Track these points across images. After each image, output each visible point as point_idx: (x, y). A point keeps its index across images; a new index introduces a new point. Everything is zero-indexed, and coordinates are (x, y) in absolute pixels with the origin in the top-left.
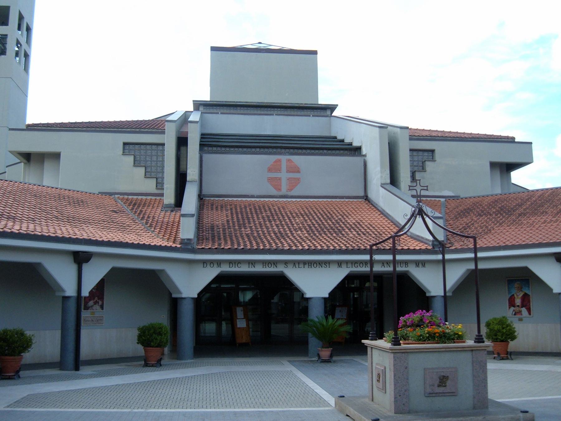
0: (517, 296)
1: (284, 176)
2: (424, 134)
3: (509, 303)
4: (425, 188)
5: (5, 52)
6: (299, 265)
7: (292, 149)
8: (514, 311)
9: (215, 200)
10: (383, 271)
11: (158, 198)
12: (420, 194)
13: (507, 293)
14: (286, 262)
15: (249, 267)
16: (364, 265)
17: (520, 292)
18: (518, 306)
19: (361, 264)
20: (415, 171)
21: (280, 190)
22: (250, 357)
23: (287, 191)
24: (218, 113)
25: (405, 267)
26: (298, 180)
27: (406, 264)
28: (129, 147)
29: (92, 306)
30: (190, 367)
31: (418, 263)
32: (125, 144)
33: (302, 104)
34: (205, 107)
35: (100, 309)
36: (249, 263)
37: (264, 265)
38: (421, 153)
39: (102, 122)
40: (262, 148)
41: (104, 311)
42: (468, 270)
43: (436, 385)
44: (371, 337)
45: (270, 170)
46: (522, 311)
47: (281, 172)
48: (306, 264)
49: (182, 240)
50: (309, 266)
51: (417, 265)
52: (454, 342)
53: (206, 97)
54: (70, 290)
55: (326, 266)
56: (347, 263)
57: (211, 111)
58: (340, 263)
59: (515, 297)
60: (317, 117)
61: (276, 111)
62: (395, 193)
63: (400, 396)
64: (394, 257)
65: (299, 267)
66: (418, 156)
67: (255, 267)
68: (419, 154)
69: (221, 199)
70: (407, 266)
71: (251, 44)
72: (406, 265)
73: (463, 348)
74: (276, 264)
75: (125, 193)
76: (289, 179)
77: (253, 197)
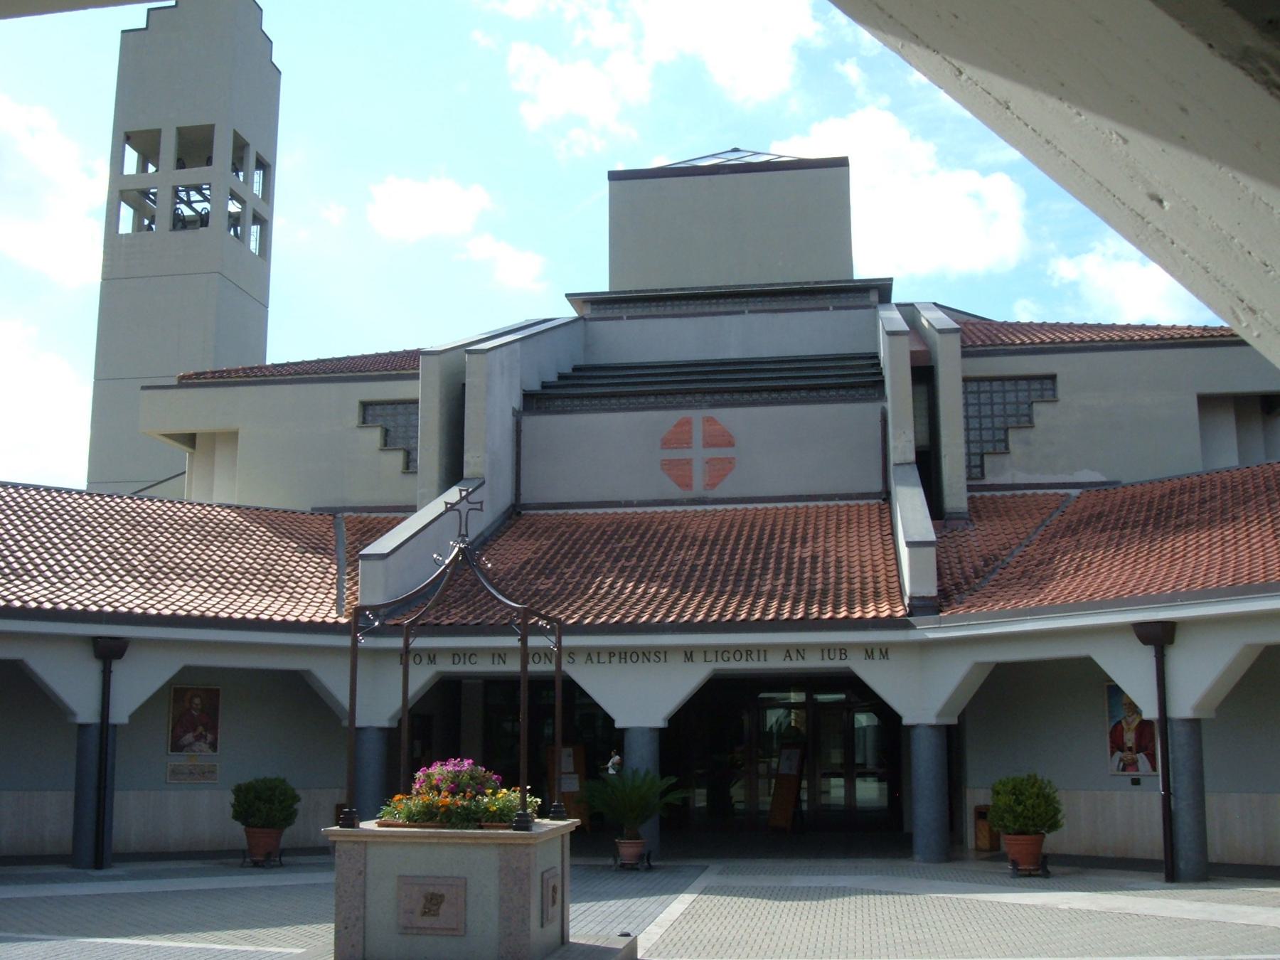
0: (1128, 724)
1: (698, 454)
2: (1115, 335)
3: (1112, 742)
5: (208, 222)
6: (705, 656)
8: (1121, 760)
13: (1107, 718)
15: (493, 663)
17: (1133, 714)
18: (1130, 749)
19: (738, 653)
21: (688, 486)
22: (845, 858)
24: (620, 318)
25: (841, 659)
27: (843, 651)
28: (991, 386)
29: (190, 744)
31: (869, 651)
32: (365, 406)
34: (595, 306)
35: (210, 750)
36: (493, 655)
40: (660, 394)
41: (218, 753)
42: (979, 665)
44: (553, 812)
45: (666, 444)
46: (1137, 761)
48: (615, 655)
50: (620, 658)
52: (481, 827)
53: (600, 283)
54: (86, 711)
55: (658, 660)
56: (705, 652)
57: (609, 313)
58: (689, 654)
59: (1123, 728)
63: (346, 928)
65: (705, 661)
67: (806, 656)
68: (1019, 388)
69: (560, 512)
70: (843, 657)
72: (841, 654)
74: (647, 655)
76: (709, 462)
77: (629, 504)
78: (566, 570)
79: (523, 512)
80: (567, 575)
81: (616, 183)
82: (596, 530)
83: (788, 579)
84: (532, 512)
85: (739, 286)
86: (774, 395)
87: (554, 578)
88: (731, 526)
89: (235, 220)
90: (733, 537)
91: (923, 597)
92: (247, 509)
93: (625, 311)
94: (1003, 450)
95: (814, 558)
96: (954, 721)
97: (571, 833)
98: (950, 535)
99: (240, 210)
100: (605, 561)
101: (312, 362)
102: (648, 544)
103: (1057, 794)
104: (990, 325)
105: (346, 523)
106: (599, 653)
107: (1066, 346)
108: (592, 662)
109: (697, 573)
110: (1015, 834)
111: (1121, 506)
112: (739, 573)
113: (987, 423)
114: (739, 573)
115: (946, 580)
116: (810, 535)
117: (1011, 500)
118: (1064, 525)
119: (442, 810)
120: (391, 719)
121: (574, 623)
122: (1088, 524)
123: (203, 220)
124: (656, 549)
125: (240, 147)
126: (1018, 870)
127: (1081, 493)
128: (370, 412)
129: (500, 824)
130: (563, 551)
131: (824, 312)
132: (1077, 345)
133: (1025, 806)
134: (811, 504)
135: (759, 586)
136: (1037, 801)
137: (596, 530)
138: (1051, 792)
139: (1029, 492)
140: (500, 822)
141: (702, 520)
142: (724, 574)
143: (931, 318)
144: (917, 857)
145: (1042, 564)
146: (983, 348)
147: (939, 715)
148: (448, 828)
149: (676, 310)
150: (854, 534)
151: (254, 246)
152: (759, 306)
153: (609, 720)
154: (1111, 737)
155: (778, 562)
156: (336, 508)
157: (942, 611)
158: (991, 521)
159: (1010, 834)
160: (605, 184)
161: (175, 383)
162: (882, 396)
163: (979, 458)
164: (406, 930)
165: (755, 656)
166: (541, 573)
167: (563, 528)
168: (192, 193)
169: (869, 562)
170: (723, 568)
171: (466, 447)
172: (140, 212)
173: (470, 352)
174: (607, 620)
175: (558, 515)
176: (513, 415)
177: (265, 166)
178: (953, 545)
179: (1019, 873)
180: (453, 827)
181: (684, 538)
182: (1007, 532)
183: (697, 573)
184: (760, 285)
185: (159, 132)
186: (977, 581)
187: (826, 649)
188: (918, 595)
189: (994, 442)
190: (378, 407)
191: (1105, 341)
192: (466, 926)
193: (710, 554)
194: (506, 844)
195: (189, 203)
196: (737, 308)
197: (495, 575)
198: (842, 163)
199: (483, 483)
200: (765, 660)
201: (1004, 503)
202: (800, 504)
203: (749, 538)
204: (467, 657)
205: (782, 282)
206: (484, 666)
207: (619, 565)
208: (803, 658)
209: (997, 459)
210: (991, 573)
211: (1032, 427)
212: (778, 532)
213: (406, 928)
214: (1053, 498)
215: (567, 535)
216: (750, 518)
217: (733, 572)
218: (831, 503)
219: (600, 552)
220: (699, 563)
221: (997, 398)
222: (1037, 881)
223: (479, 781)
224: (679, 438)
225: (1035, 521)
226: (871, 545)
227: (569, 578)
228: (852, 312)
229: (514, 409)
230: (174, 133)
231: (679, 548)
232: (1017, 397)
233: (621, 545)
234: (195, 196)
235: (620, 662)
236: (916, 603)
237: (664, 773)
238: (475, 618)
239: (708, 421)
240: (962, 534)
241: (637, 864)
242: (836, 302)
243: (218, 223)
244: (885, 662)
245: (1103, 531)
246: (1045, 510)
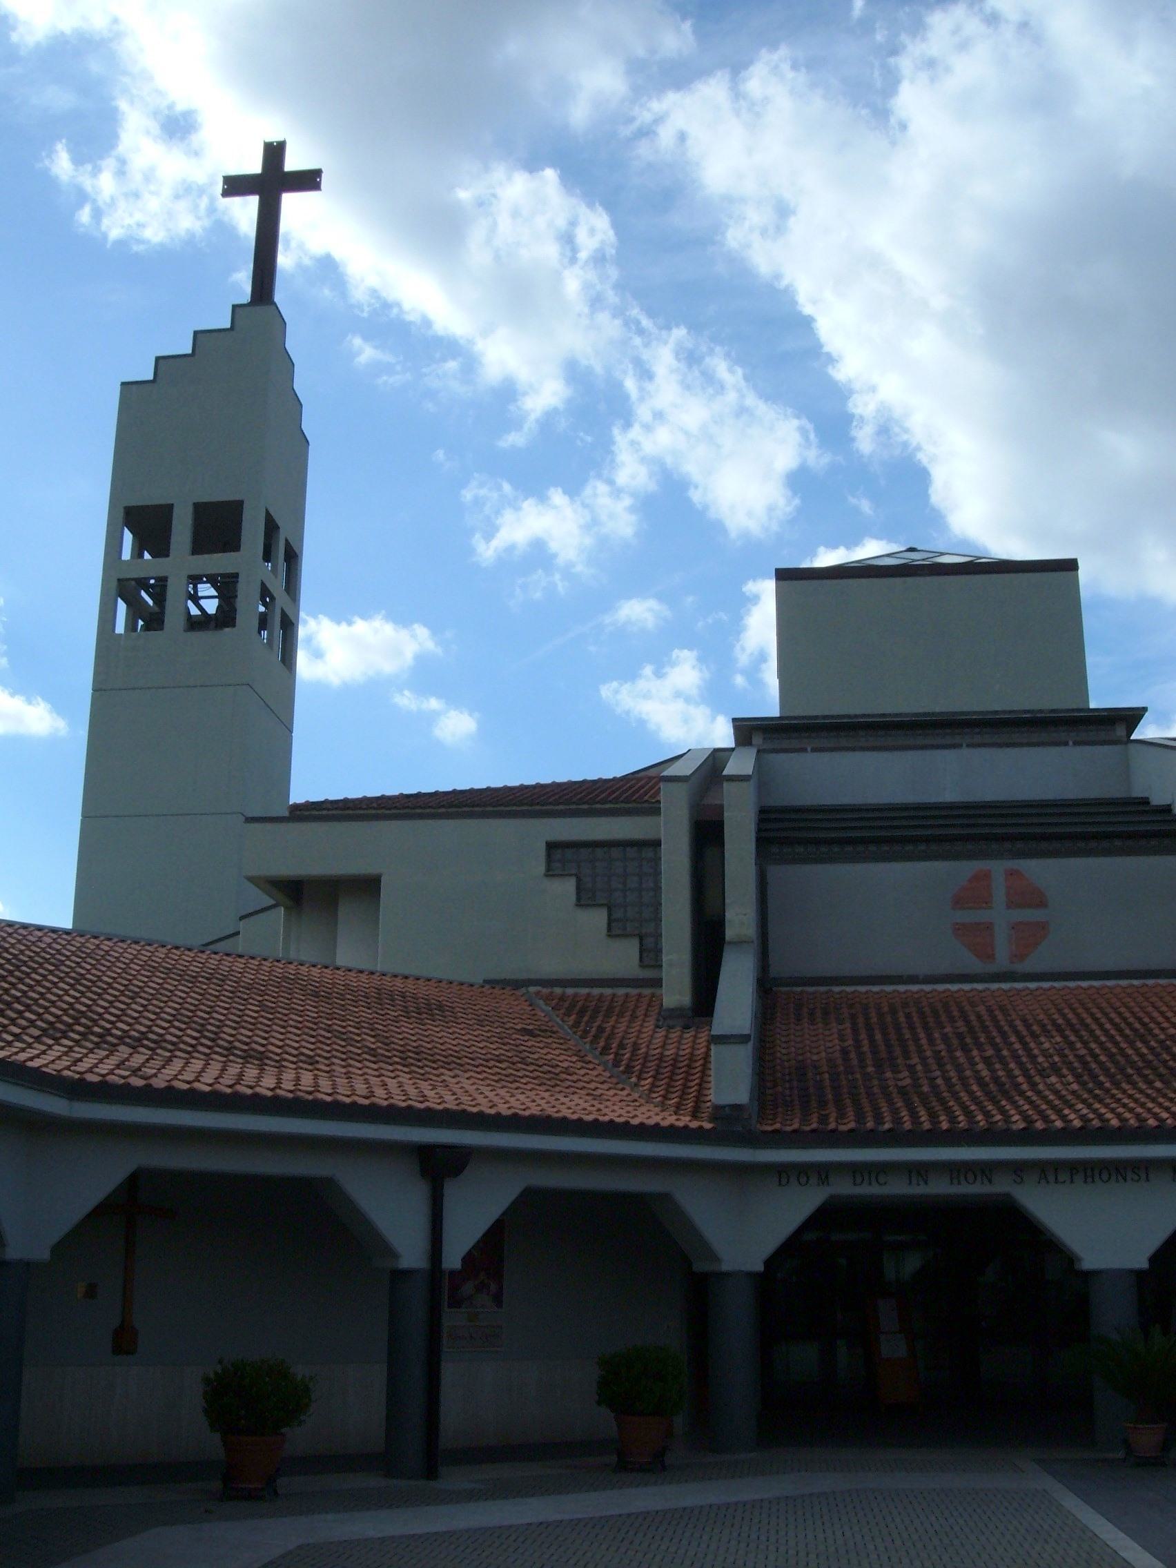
1: (1000, 916)
11: (647, 992)
14: (1018, 1169)
21: (991, 957)
23: (1012, 962)
24: (803, 750)
26: (1041, 929)
32: (551, 847)
33: (1041, 711)
50: (1086, 1176)
76: (1015, 927)
77: (913, 980)
81: (786, 584)
101: (411, 795)
106: (1147, 1168)
108: (1048, 1182)
125: (271, 527)
131: (1062, 749)
152: (977, 739)
153: (1069, 1260)
156: (517, 981)
161: (287, 814)
172: (136, 609)
185: (170, 507)
198: (1070, 566)
204: (1096, 1172)
206: (939, 1187)
208: (990, 1181)
230: (190, 510)
235: (952, 1183)
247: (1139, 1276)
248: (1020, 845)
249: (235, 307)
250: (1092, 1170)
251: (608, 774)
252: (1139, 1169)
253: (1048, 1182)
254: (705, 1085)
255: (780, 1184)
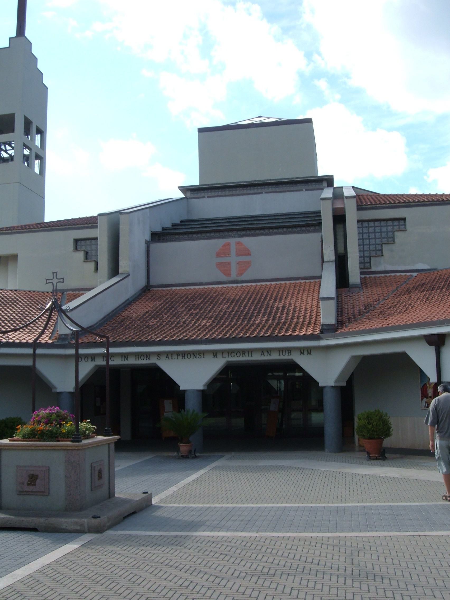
1: (233, 259)
3: (422, 394)
4: (62, 280)
7: (262, 229)
8: (426, 402)
9: (386, 276)
10: (135, 364)
11: (317, 280)
12: (56, 288)
14: (159, 354)
15: (136, 360)
16: (242, 355)
18: (431, 397)
19: (238, 353)
20: (383, 244)
21: (229, 275)
23: (237, 276)
24: (204, 197)
26: (248, 264)
27: (289, 351)
28: (374, 224)
30: (335, 461)
31: (302, 350)
32: (76, 241)
33: (293, 178)
34: (192, 192)
37: (137, 357)
38: (390, 223)
39: (72, 219)
42: (354, 357)
43: (26, 484)
44: (105, 432)
47: (230, 256)
49: (60, 335)
50: (182, 357)
51: (309, 352)
52: (59, 441)
53: (195, 181)
55: (200, 357)
56: (223, 353)
57: (199, 195)
58: (215, 353)
60: (310, 191)
61: (267, 189)
62: (117, 284)
64: (77, 351)
65: (172, 359)
66: (387, 226)
67: (128, 359)
69: (169, 288)
70: (290, 354)
71: (249, 120)
73: (61, 446)
74: (195, 355)
75: (77, 289)
77: (201, 284)
78: (165, 315)
79: (151, 289)
80: (164, 318)
81: (202, 133)
82: (184, 296)
83: (269, 317)
84: (155, 289)
85: (260, 181)
86: (271, 231)
87: (158, 319)
88: (248, 293)
89: (26, 158)
90: (247, 299)
91: (328, 324)
92: (43, 292)
93: (206, 194)
94: (381, 255)
95: (284, 307)
96: (344, 384)
97: (115, 442)
98: (351, 295)
99: (29, 153)
100: (184, 311)
102: (206, 303)
103: (389, 419)
104: (378, 196)
105: (67, 297)
107: (411, 204)
108: (264, 356)
109: (226, 315)
110: (369, 439)
111: (434, 280)
112: (246, 315)
113: (373, 241)
114: (246, 315)
115: (344, 316)
116: (284, 297)
117: (383, 278)
118: (405, 290)
119: (39, 432)
120: (204, 385)
121: (160, 340)
122: (417, 288)
123: (11, 158)
124: (209, 305)
125: (28, 124)
126: (370, 456)
127: (418, 275)
128: (79, 244)
129: (68, 439)
130: (165, 307)
131: (301, 192)
132: (416, 204)
133: (373, 425)
134: (288, 282)
135: (254, 320)
136: (379, 423)
137: (184, 296)
138: (387, 418)
139: (393, 274)
140: (68, 438)
141: (235, 290)
142: (239, 315)
143: (348, 192)
144: (326, 450)
145: (391, 308)
146: (371, 206)
147: (336, 382)
148: (42, 441)
149: (231, 193)
150: (305, 296)
151: (37, 170)
152: (270, 190)
154: (422, 391)
155: (266, 309)
156: (63, 290)
157: (337, 331)
158: (373, 288)
159: (366, 439)
160: (197, 134)
162: (321, 231)
163: (369, 258)
164: (21, 493)
165: (247, 354)
166: (152, 317)
167: (169, 296)
168: (7, 146)
169: (310, 309)
170: (239, 313)
171: (120, 258)
173: (122, 214)
174: (182, 338)
175: (167, 290)
176: (146, 243)
177: (41, 132)
178: (351, 300)
179: (371, 458)
180: (44, 441)
181: (225, 298)
182: (378, 293)
183: (226, 315)
184: (270, 180)
186: (359, 317)
187: (281, 350)
188: (325, 324)
189: (376, 250)
190: (82, 242)
191: (430, 202)
192: (49, 490)
193: (235, 306)
194: (68, 449)
195: (6, 151)
196: (260, 191)
197: (131, 319)
198: (309, 121)
199: (129, 275)
200: (252, 356)
201: (380, 280)
202: (283, 282)
203: (255, 299)
204: (186, 355)
205: (281, 178)
206: (132, 361)
207: (190, 312)
208: (270, 355)
209: (377, 259)
210: (367, 313)
211: (394, 243)
212: (269, 296)
213: (20, 492)
214: (404, 277)
215: (169, 299)
216: (257, 289)
217: (244, 314)
218: (297, 282)
219: (183, 306)
220: (228, 310)
221: (378, 230)
222: (381, 462)
223: (61, 418)
224: (224, 252)
225: (393, 288)
226: (307, 301)
227: (165, 319)
228: (315, 191)
229: (146, 240)
231: (221, 304)
232: (387, 229)
233: (193, 303)
234: (8, 148)
235: (136, 360)
236: (324, 327)
237: (204, 411)
238: (145, 338)
239: (238, 244)
240: (357, 295)
241: (188, 455)
242: (307, 187)
243: (18, 159)
244: (309, 356)
245: (423, 291)
246: (399, 283)
247: (202, 392)
248: (244, 232)
249: (10, 38)
250: (138, 356)
251: (382, 192)
252: (201, 354)
253: (264, 356)
254: (318, 317)
255: (223, 357)
